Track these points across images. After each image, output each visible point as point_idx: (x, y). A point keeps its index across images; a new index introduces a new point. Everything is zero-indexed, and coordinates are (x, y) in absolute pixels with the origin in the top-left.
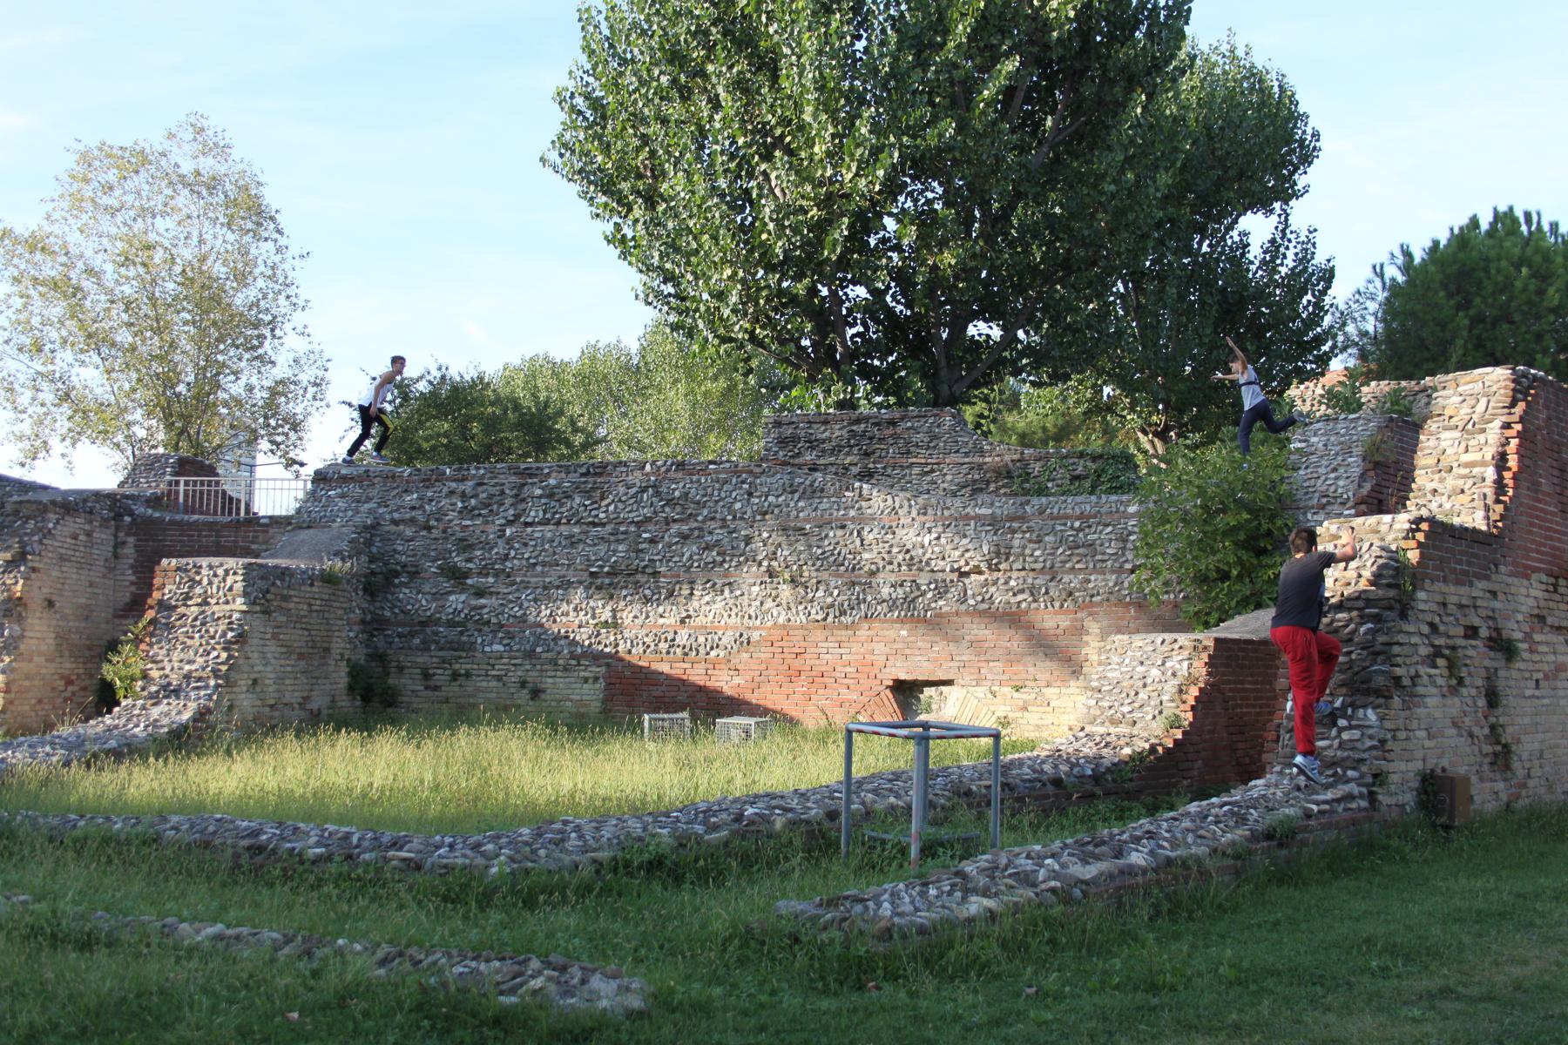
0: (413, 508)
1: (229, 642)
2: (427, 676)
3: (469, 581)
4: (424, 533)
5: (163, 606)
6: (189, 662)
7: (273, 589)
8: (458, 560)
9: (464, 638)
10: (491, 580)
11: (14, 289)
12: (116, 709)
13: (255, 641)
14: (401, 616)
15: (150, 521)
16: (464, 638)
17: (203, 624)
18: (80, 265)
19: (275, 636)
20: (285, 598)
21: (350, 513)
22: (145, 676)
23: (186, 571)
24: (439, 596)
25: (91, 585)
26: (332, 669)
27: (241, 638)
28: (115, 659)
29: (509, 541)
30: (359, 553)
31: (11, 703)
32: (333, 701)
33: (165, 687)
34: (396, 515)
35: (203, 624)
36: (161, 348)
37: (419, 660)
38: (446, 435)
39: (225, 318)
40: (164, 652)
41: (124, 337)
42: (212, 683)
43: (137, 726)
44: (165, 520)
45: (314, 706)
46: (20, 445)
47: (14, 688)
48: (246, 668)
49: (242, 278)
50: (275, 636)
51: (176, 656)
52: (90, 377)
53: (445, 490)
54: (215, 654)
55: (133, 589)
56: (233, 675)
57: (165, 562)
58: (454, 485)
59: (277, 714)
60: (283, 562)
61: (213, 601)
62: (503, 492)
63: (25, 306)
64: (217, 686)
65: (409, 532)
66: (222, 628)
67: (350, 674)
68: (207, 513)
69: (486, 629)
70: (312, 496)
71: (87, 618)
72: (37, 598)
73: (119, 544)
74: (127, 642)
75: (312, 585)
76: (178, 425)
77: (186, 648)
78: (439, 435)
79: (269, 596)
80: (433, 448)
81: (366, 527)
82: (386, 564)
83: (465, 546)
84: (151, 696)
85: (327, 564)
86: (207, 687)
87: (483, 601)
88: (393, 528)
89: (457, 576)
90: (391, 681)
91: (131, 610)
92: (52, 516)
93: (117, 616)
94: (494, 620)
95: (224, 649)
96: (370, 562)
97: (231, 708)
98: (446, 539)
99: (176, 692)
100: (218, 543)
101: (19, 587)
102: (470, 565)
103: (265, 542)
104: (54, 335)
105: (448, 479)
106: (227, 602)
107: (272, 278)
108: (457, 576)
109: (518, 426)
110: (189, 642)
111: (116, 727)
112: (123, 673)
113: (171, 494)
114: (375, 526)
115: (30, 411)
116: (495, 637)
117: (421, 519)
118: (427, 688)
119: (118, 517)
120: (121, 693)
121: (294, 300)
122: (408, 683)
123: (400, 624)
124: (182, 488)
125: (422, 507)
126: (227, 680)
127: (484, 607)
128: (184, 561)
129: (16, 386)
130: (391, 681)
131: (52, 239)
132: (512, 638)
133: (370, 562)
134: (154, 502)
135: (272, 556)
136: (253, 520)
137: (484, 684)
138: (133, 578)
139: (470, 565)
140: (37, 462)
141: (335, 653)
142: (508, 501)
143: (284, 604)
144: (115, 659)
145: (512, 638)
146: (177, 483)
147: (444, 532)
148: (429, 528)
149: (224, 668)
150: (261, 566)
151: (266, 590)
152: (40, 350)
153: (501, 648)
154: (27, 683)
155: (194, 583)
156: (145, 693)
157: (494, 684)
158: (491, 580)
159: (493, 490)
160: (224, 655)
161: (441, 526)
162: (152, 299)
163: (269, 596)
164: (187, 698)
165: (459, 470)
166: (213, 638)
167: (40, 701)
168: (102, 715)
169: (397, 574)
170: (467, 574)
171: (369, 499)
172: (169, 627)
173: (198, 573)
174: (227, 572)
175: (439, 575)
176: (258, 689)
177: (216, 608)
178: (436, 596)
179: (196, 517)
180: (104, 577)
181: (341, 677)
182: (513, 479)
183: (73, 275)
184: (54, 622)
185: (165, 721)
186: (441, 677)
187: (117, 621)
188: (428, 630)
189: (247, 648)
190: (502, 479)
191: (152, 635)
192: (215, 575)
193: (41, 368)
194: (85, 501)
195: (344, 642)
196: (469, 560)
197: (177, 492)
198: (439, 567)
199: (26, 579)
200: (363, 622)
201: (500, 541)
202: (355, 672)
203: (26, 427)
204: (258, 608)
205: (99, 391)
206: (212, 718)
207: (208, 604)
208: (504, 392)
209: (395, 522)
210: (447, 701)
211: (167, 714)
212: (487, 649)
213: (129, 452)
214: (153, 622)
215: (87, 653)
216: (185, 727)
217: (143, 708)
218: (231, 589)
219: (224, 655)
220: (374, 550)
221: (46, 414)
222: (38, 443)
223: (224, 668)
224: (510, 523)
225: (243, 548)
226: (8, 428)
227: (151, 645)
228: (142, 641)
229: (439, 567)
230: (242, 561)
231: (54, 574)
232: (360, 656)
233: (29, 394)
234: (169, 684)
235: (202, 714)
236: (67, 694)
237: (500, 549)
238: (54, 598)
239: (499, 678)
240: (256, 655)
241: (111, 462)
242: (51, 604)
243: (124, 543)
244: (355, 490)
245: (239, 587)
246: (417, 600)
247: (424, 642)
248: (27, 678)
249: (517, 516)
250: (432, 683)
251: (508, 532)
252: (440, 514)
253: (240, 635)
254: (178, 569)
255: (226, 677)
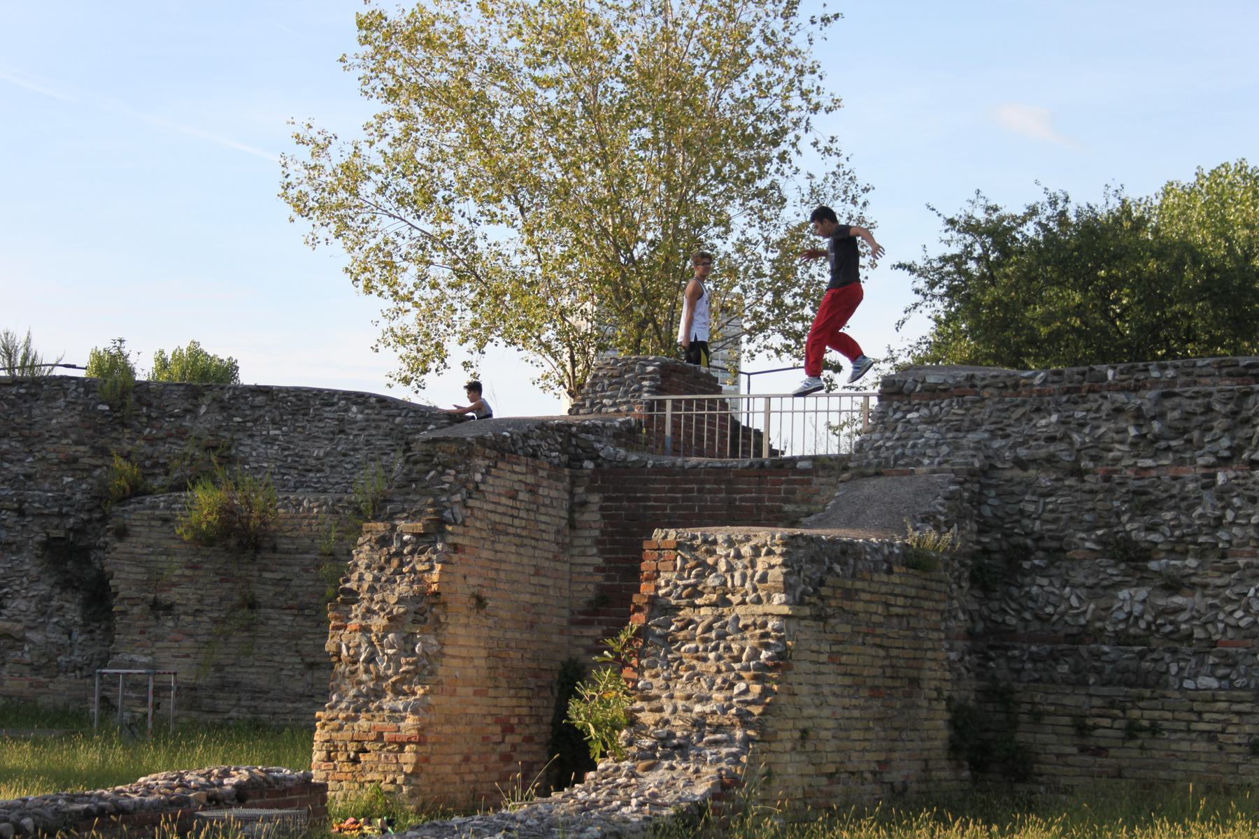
0: (1051, 439)
1: (764, 667)
2: (1082, 729)
3: (1153, 565)
4: (1070, 481)
5: (659, 607)
6: (703, 699)
7: (830, 580)
8: (1133, 528)
9: (1146, 665)
10: (1192, 562)
11: (390, 108)
12: (590, 775)
13: (805, 666)
14: (1036, 625)
15: (623, 468)
16: (1146, 665)
17: (722, 637)
18: (481, 61)
19: (834, 658)
20: (849, 594)
21: (945, 449)
22: (632, 722)
23: (692, 549)
24: (1102, 590)
25: (538, 571)
26: (923, 713)
27: (782, 660)
28: (588, 693)
29: (1223, 495)
30: (961, 517)
31: (427, 760)
32: (926, 769)
33: (664, 740)
34: (1022, 452)
35: (722, 637)
36: (608, 186)
37: (1067, 701)
38: (1079, 311)
39: (704, 125)
40: (660, 682)
41: (551, 171)
42: (739, 734)
43: (627, 803)
44: (645, 464)
45: (896, 776)
46: (402, 351)
47: (431, 737)
48: (791, 712)
49: (734, 65)
50: (834, 658)
51: (679, 689)
52: (502, 239)
53: (1107, 406)
54: (741, 686)
55: (599, 578)
56: (771, 721)
57: (658, 534)
58: (1121, 397)
59: (838, 789)
60: (844, 534)
61: (736, 599)
62: (1209, 409)
63: (407, 132)
64: (747, 740)
65: (1045, 481)
66: (750, 644)
67: (952, 723)
68: (722, 454)
69: (1184, 648)
70: (881, 419)
71: (532, 626)
72: (461, 594)
73: (577, 506)
74: (606, 664)
75: (890, 571)
76: (640, 311)
77: (695, 676)
78: (1066, 313)
79: (824, 591)
80: (1055, 336)
81: (972, 473)
82: (1007, 536)
83: (1144, 503)
84: (644, 754)
85: (912, 537)
86: (730, 741)
87: (1178, 600)
88: (1017, 473)
89: (1132, 556)
90: (1020, 737)
91: (596, 612)
92: (480, 462)
93: (573, 623)
94: (1199, 633)
95: (756, 679)
96: (981, 532)
97: (769, 774)
98: (1110, 491)
99: (682, 749)
100: (731, 502)
101: (435, 576)
102: (1154, 537)
103: (807, 501)
104: (448, 176)
105: (1110, 388)
106: (758, 601)
107: (776, 59)
108: (1132, 556)
109: (1205, 290)
110: (700, 666)
111: (594, 804)
112: (600, 716)
113: (652, 421)
114: (988, 470)
115: (416, 297)
116: (1201, 663)
117: (1066, 457)
118: (1083, 750)
119: (574, 461)
120: (597, 748)
121: (814, 98)
122: (1051, 742)
123: (1032, 639)
124: (669, 411)
125: (1066, 437)
126: (761, 728)
127: (1181, 609)
128: (688, 532)
129: (397, 259)
130: (1020, 737)
131: (439, 26)
132: (1233, 666)
133: (981, 532)
134: (628, 435)
135: (820, 523)
136: (783, 466)
137: (1185, 746)
138: (599, 561)
139: (1154, 537)
140: (427, 378)
141: (929, 686)
142: (1219, 424)
143: (847, 605)
144: (588, 693)
145: (1233, 666)
146: (662, 404)
147: (1107, 479)
148: (1079, 473)
149: (757, 710)
150: (810, 540)
151: (819, 579)
152: (430, 200)
153: (1215, 684)
154: (448, 729)
155: (707, 569)
156: (634, 750)
157: (1201, 746)
158: (1192, 562)
159: (1190, 405)
160: (756, 689)
161: (1101, 469)
162: (591, 113)
163: (824, 591)
164: (701, 758)
165: (1129, 371)
166: (737, 659)
167: (467, 759)
168: (571, 785)
169: (1027, 553)
170: (1148, 553)
171: (975, 426)
172: (668, 641)
173: (711, 553)
174: (756, 550)
175: (1102, 554)
176: (809, 746)
177: (740, 610)
178: (1094, 591)
179: (694, 460)
180: (556, 558)
181: (938, 729)
182: (1227, 384)
183: (472, 78)
184: (485, 632)
185: (669, 797)
186: (1107, 730)
187: (576, 631)
188: (1083, 650)
189: (792, 678)
190: (1206, 385)
191: (641, 654)
192: (739, 556)
193: (429, 229)
194: (526, 437)
195: (942, 668)
196: (1151, 528)
197: (662, 420)
198: (1099, 541)
199: (443, 562)
200: (970, 634)
201: (1206, 495)
202: (960, 720)
203: (410, 321)
204: (807, 611)
205: (516, 260)
206: (739, 793)
207: (729, 603)
208: (1174, 232)
209: (1021, 464)
210: (1119, 775)
211: (670, 785)
212: (1188, 684)
213: (566, 357)
214: (642, 632)
215: (532, 682)
216: (699, 808)
217: (632, 774)
218: (764, 579)
219: (756, 689)
220: (987, 511)
221: (440, 300)
222: (428, 348)
223: (757, 710)
224: (1223, 462)
225: (770, 510)
226: (385, 324)
227: (640, 670)
228: (625, 664)
229: (1099, 541)
230: (780, 532)
231: (485, 554)
232: (967, 692)
233: (414, 269)
234: (671, 735)
235: (724, 786)
236: (505, 748)
237: (1207, 508)
238: (486, 593)
239: (1211, 736)
240: (805, 689)
241: (538, 373)
242: (480, 602)
243: (584, 504)
244: (951, 409)
245: (777, 574)
246: (1063, 597)
247: (1075, 671)
248: (448, 722)
249: (1236, 451)
250: (1091, 742)
251: (1221, 478)
252: (1099, 449)
253: (780, 656)
254: (679, 546)
255: (760, 725)
